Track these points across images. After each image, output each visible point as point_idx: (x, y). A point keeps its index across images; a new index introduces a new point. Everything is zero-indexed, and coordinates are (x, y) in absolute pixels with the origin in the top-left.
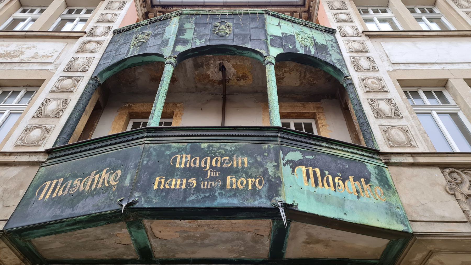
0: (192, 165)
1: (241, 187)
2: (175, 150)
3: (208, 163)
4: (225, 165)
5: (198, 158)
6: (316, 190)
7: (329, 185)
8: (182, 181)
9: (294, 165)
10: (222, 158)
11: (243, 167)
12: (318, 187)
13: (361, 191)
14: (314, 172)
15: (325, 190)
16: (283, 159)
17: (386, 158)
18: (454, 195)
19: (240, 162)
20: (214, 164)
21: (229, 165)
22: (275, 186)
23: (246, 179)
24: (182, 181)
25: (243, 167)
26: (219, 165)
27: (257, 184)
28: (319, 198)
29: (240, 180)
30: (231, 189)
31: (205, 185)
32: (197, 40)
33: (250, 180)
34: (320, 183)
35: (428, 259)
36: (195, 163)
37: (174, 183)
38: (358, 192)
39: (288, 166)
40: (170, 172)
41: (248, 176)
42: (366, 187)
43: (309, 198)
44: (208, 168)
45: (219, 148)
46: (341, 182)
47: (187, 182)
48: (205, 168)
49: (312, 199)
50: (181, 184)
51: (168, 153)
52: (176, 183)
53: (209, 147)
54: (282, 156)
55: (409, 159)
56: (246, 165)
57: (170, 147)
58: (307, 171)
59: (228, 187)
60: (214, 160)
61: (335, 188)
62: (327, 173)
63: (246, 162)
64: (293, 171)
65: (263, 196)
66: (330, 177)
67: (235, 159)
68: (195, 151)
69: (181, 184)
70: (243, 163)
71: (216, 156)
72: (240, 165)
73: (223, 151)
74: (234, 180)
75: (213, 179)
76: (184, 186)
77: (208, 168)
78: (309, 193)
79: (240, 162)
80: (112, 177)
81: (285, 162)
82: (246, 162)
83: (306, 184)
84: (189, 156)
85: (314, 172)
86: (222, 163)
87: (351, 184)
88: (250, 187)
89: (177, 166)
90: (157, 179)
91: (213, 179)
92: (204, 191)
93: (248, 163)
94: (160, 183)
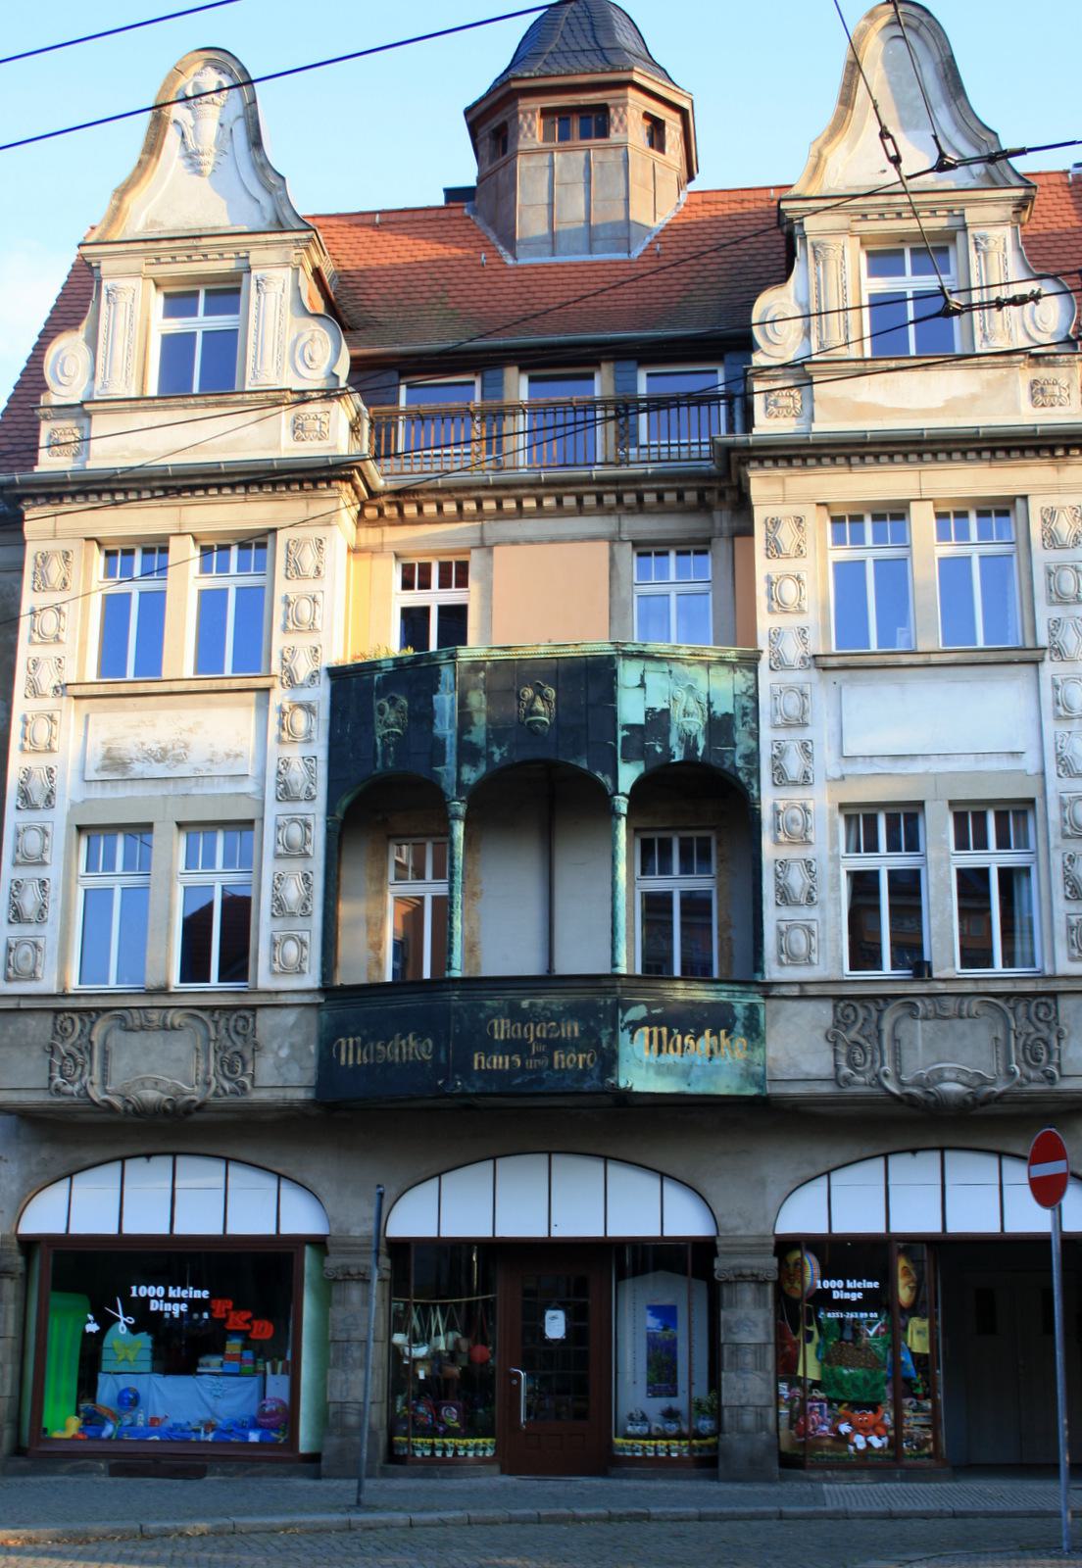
0: (514, 1035)
1: (570, 1066)
2: (491, 1012)
3: (535, 1032)
4: (551, 1036)
5: (519, 1025)
6: (658, 1060)
7: (675, 1049)
8: (504, 1059)
9: (634, 1026)
10: (547, 1023)
11: (573, 1038)
12: (662, 1056)
13: (716, 1051)
14: (660, 1034)
15: (671, 1057)
16: (622, 1020)
17: (766, 989)
18: (835, 1044)
19: (569, 1029)
20: (538, 1035)
21: (557, 1035)
22: (609, 1061)
23: (576, 1054)
24: (504, 1059)
25: (573, 1038)
26: (544, 1035)
27: (588, 1061)
28: (662, 1070)
29: (569, 1058)
30: (560, 1068)
31: (530, 1064)
32: (495, 749)
33: (581, 1056)
34: (664, 1048)
35: (359, 1245)
36: (516, 1032)
37: (495, 1061)
38: (712, 1052)
39: (627, 1032)
40: (490, 1047)
41: (580, 1050)
42: (724, 1042)
43: (647, 1071)
44: (532, 1039)
45: (544, 1009)
46: (692, 1042)
47: (510, 1061)
48: (529, 1039)
49: (652, 1072)
50: (504, 1064)
51: (482, 1015)
52: (499, 1062)
53: (532, 1005)
54: (620, 1016)
55: (795, 991)
56: (576, 1034)
57: (483, 1006)
58: (651, 1033)
59: (556, 1066)
60: (538, 1028)
61: (682, 1051)
62: (676, 1031)
63: (576, 1029)
64: (632, 1039)
65: (594, 1076)
66: (679, 1037)
67: (563, 1025)
68: (516, 1014)
69: (504, 1064)
70: (573, 1031)
71: (541, 1022)
72: (569, 1035)
73: (549, 1014)
74: (562, 1056)
75: (538, 1055)
76: (507, 1066)
77: (532, 1039)
78: (649, 1064)
79: (569, 1029)
80: (423, 1049)
81: (623, 1025)
82: (576, 1029)
83: (646, 1054)
84: (508, 1021)
85: (660, 1034)
86: (548, 1032)
87: (706, 1040)
88: (581, 1066)
89: (496, 1037)
90: (476, 1056)
91: (538, 1055)
92: (532, 1071)
93: (580, 1031)
94: (480, 1062)
